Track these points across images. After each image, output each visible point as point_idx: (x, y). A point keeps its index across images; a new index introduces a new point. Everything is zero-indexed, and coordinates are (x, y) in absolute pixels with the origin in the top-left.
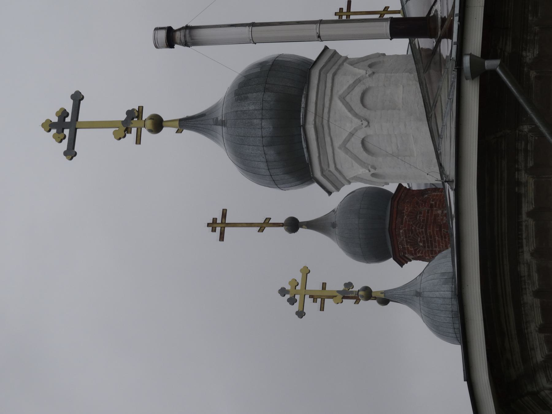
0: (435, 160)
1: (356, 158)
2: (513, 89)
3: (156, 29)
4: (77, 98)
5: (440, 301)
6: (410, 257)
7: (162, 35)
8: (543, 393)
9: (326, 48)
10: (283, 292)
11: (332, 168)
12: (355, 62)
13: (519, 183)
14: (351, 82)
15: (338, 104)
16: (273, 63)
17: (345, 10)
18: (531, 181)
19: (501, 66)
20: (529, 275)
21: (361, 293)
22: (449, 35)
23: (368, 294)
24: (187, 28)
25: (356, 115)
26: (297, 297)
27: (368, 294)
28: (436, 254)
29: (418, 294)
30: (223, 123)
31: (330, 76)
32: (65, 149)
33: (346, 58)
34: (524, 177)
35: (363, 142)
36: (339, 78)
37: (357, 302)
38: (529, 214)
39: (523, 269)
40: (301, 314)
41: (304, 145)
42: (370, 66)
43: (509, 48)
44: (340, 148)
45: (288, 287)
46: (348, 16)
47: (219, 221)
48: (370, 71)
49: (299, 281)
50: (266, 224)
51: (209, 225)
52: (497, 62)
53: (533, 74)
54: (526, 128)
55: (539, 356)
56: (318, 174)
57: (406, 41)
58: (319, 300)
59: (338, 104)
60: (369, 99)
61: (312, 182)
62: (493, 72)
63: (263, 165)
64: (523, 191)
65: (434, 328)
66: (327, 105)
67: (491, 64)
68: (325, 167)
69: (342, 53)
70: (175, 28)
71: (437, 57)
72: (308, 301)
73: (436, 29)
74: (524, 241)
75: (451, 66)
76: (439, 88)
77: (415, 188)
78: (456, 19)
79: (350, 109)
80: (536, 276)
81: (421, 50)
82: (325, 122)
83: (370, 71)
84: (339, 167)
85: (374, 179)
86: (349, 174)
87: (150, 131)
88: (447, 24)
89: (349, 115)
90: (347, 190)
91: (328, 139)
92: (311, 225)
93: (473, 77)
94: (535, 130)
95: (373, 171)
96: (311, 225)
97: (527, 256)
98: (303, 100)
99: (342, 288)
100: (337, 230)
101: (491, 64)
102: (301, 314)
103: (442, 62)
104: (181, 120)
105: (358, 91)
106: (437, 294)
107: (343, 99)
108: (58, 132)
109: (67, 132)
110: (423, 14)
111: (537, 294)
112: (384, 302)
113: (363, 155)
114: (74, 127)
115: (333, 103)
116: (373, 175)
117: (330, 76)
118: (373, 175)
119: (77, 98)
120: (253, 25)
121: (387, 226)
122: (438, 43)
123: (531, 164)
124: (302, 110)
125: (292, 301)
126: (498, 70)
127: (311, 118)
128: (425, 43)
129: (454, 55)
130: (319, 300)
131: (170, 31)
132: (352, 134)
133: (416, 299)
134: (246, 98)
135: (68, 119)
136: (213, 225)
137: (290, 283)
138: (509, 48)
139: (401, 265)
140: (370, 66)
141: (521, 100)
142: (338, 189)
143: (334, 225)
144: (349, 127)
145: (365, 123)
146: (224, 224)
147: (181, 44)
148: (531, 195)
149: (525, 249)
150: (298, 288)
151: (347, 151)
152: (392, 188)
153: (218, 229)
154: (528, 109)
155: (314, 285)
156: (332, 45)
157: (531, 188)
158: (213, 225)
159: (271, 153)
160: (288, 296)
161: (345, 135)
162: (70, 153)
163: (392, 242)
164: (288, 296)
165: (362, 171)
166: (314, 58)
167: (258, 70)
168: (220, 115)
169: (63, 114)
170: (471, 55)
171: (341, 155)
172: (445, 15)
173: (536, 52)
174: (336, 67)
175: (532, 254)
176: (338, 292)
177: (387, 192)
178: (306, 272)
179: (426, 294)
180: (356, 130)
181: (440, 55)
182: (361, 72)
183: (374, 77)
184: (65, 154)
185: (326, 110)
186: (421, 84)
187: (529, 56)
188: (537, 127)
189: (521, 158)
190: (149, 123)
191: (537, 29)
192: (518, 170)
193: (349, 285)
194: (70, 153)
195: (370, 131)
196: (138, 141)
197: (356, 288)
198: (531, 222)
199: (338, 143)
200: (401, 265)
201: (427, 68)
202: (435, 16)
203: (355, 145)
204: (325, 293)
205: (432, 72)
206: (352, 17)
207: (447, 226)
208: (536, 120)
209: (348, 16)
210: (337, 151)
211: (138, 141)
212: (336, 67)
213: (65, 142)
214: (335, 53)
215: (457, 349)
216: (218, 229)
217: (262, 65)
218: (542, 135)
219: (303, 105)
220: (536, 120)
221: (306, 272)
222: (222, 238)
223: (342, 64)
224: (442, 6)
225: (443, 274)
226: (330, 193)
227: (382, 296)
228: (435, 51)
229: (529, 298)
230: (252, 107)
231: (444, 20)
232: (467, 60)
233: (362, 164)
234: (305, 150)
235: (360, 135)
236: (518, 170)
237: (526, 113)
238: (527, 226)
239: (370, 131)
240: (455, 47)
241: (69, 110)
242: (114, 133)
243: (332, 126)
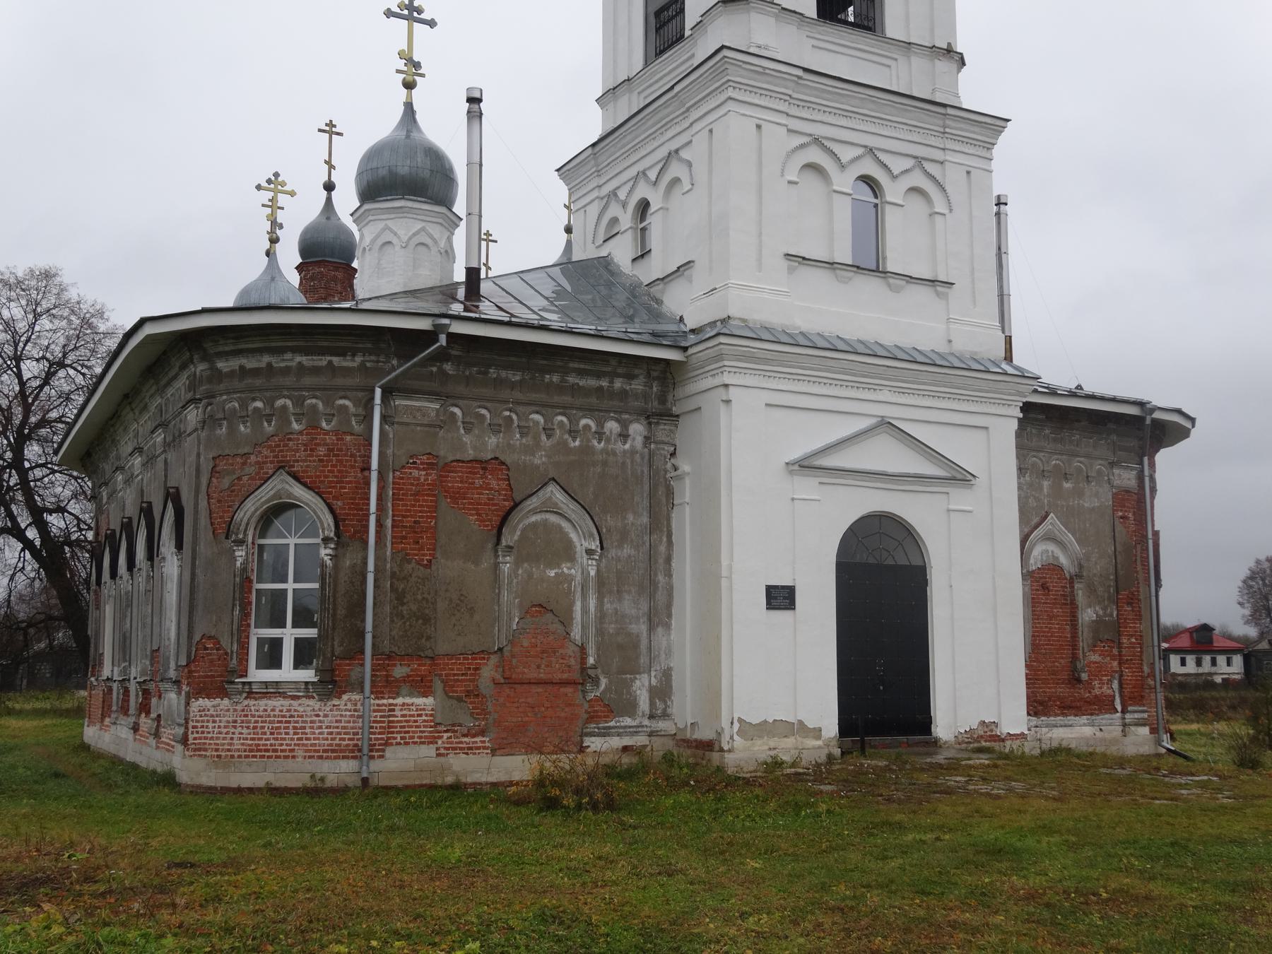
0: (374, 295)
1: (377, 237)
2: (424, 354)
3: (481, 90)
4: (431, 23)
5: (267, 295)
6: (302, 275)
7: (477, 95)
8: (192, 366)
9: (461, 219)
10: (276, 175)
11: (371, 218)
12: (450, 240)
13: (354, 355)
14: (435, 236)
15: (419, 225)
16: (451, 178)
17: (490, 238)
18: (355, 365)
19: (442, 346)
20: (283, 360)
21: (274, 235)
22: (466, 310)
23: (274, 240)
24: (481, 114)
25: (410, 239)
26: (272, 186)
27: (274, 240)
28: (305, 295)
29: (273, 279)
30: (408, 136)
31: (440, 221)
32: (393, 10)
33: (453, 234)
34: (359, 359)
35: (389, 243)
36: (438, 227)
37: (268, 233)
38: (330, 362)
39: (288, 356)
40: (259, 187)
41: (389, 198)
42: (446, 252)
43: (454, 352)
44: (386, 225)
45: (280, 179)
46: (484, 240)
47: (334, 129)
48: (442, 251)
49: (285, 188)
50: (331, 167)
51: (331, 121)
52: (444, 343)
53: (434, 369)
54: (395, 362)
55: (221, 365)
56: (366, 206)
57: (464, 280)
58: (270, 204)
59: (419, 225)
60: (421, 248)
61: (360, 202)
62: (437, 341)
63: (375, 165)
64: (348, 358)
65: (482, 465)
66: (419, 217)
67: (443, 339)
68: (372, 212)
69: (457, 231)
70: (481, 104)
71: (451, 300)
72: (272, 194)
73: (471, 301)
74: (310, 358)
75: (443, 310)
76: (427, 301)
77: (355, 281)
78: (477, 316)
79: (414, 235)
80: (282, 365)
81: (457, 289)
82: (405, 215)
83: (442, 251)
84: (372, 223)
85: (361, 248)
86: (365, 231)
87: (404, 79)
88: (475, 309)
89: (411, 233)
90: (354, 228)
91: (393, 216)
92: (329, 200)
93: (434, 325)
94: (394, 369)
95: (367, 248)
96: (329, 200)
97: (298, 359)
98: (423, 199)
99: (279, 221)
100: (324, 220)
101: (443, 339)
102: (259, 187)
103: (447, 304)
104: (412, 104)
105: (428, 241)
106: (273, 293)
107: (423, 229)
108: (406, 5)
109: (406, 12)
110: (482, 292)
111: (269, 365)
112: (268, 254)
113: (380, 242)
114: (409, 18)
115: (420, 222)
116: (364, 249)
117: (440, 221)
118: (364, 249)
119: (431, 23)
120: (481, 165)
121: (327, 259)
122: (461, 302)
123: (368, 365)
124: (415, 198)
125: (269, 181)
126: (438, 344)
127: (410, 204)
128: (461, 293)
129: (451, 312)
130: (270, 204)
131: (479, 100)
132: (395, 234)
133: (270, 277)
134: (427, 156)
135: (415, 14)
136: (331, 124)
137: (283, 181)
138: (454, 352)
139: (297, 268)
140: (446, 252)
141: (415, 360)
142: (354, 221)
143: (328, 218)
144: (401, 232)
145: (404, 245)
146: (331, 133)
147: (469, 108)
148: (345, 364)
149: (304, 358)
150: (280, 187)
151: (384, 230)
152: (355, 264)
153: (327, 128)
154: (409, 364)
155: (283, 200)
156: (463, 224)
157: (350, 364)
158: (331, 124)
159: (383, 172)
160: (273, 178)
161: (394, 229)
162: (389, 13)
163: (317, 261)
164: (273, 178)
165: (367, 240)
166: (453, 210)
167: (447, 167)
168: (414, 134)
169: (420, 11)
170: (450, 325)
171: (381, 225)
172: (481, 308)
173: (450, 372)
174: (447, 225)
175: (300, 363)
176: (276, 218)
177: (352, 260)
178: (292, 194)
179: (273, 285)
180: (399, 237)
181: (452, 303)
182: (442, 244)
183: (439, 254)
184: (389, 9)
185: (415, 216)
186: (432, 288)
187: (448, 367)
188: (395, 370)
189: (373, 358)
190: (410, 78)
191: (467, 373)
192: (364, 355)
193: (281, 226)
194: (389, 13)
195: (397, 248)
196: (398, 71)
197: (278, 232)
198: (324, 363)
199: (390, 223)
200: (297, 268)
201: (443, 293)
202: (480, 301)
203: (388, 236)
204: (274, 208)
205: (441, 296)
206: (484, 244)
207: (325, 300)
208: (401, 369)
209: (484, 240)
210: (384, 223)
211: (398, 71)
212: (447, 225)
213: (398, 10)
214: (458, 226)
215: (231, 305)
216: (327, 128)
217: (451, 170)
218: (389, 373)
219: (419, 199)
220: (401, 369)
221: (292, 194)
222: (320, 130)
223: (449, 231)
224: (487, 306)
225: (288, 298)
226: (352, 215)
227: (272, 252)
228: (455, 299)
229: (266, 359)
230: (419, 160)
231: (477, 307)
232: (446, 321)
233: (373, 241)
234: (385, 198)
235: (395, 241)
236: (364, 355)
237: (406, 363)
238: (321, 360)
239: (397, 248)
240: (457, 313)
241: (422, 16)
242: (404, 50)
243: (402, 220)
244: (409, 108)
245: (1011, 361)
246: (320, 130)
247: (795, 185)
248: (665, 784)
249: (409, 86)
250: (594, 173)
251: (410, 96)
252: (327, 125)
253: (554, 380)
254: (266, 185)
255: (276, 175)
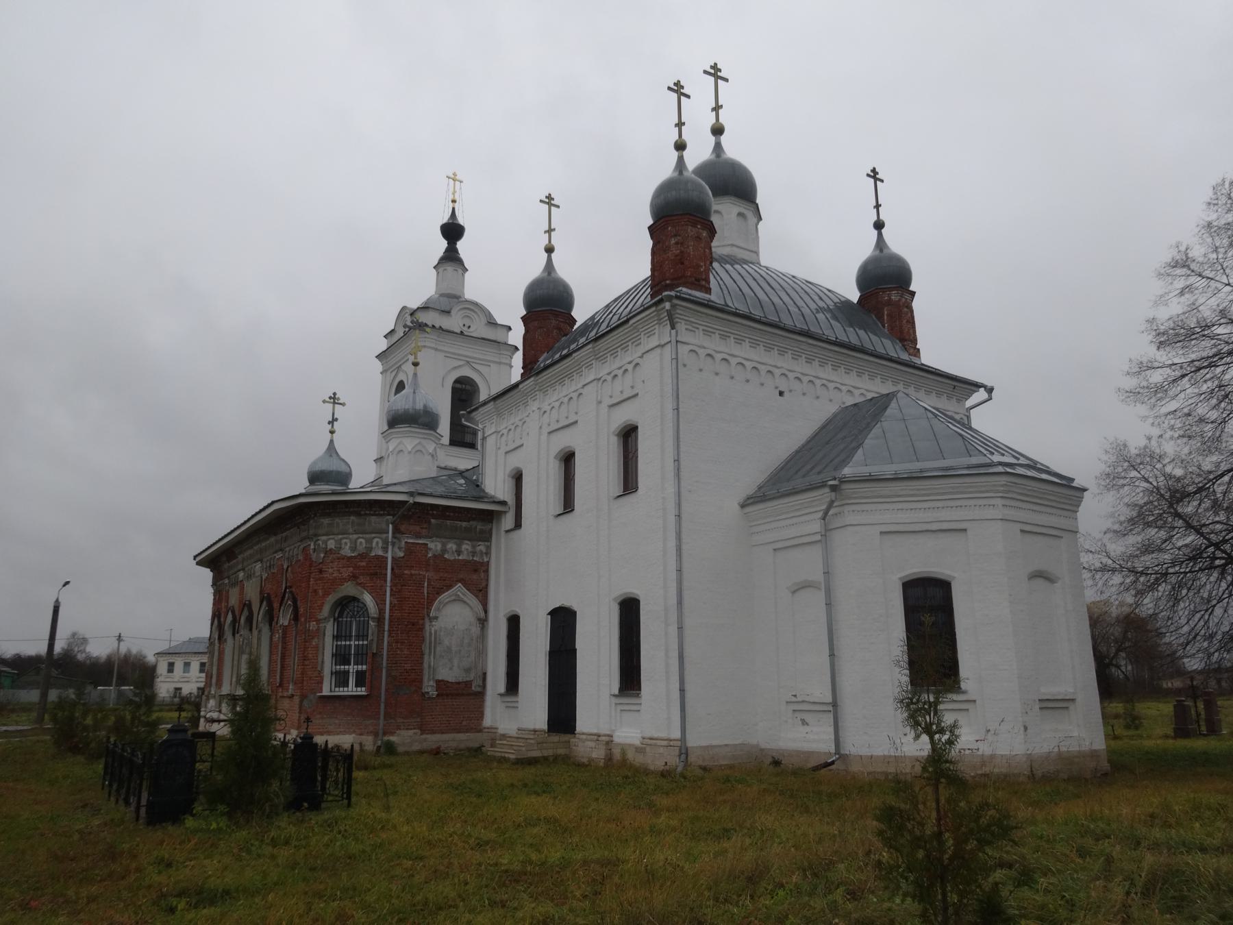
4: (343, 404)
15: (417, 441)
35: (402, 451)
92: (549, 260)
96: (549, 260)
113: (397, 450)
119: (343, 404)
136: (549, 197)
139: (521, 318)
158: (549, 197)
166: (438, 431)
200: (521, 318)
203: (400, 447)
222: (541, 201)
241: (340, 402)
244: (332, 441)
245: (904, 330)
246: (541, 201)
247: (522, 448)
248: (968, 889)
249: (332, 432)
250: (532, 385)
251: (332, 437)
252: (546, 197)
253: (156, 758)
254: (329, 400)
255: (335, 394)
